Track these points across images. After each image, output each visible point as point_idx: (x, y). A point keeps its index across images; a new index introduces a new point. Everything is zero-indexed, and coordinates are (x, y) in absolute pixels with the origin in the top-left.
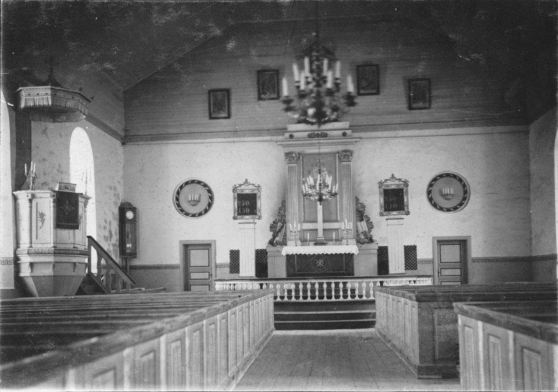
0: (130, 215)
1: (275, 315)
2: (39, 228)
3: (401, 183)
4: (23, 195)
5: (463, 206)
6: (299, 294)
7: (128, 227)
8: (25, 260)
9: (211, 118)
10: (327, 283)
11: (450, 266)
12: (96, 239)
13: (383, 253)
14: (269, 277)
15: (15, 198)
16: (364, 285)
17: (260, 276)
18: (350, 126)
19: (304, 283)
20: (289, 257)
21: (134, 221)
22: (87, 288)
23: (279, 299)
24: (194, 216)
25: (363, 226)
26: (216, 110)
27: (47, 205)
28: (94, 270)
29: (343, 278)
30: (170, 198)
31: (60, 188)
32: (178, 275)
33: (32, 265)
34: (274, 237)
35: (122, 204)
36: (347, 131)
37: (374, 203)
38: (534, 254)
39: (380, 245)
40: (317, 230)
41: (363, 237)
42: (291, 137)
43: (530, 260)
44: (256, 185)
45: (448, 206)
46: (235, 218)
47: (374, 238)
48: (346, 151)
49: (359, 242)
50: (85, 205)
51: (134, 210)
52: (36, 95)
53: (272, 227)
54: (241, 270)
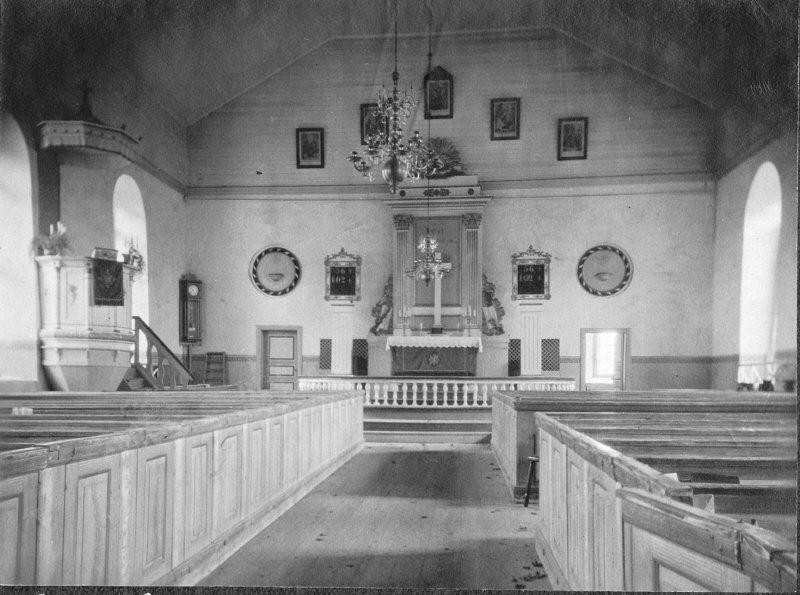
0: (193, 290)
1: (365, 423)
6: (412, 397)
7: (190, 307)
8: (51, 345)
9: (299, 166)
12: (147, 323)
13: (515, 345)
14: (369, 375)
15: (38, 266)
16: (485, 388)
17: (360, 374)
18: (479, 182)
20: (394, 349)
21: (198, 299)
22: (135, 383)
23: (368, 404)
25: (491, 312)
26: (305, 155)
27: (82, 280)
28: (143, 361)
30: (246, 267)
31: (97, 254)
32: (255, 367)
33: (60, 351)
35: (184, 276)
37: (507, 281)
38: (716, 353)
40: (433, 316)
41: (490, 326)
43: (709, 361)
47: (504, 329)
49: (486, 332)
51: (198, 283)
52: (59, 134)
53: (376, 311)
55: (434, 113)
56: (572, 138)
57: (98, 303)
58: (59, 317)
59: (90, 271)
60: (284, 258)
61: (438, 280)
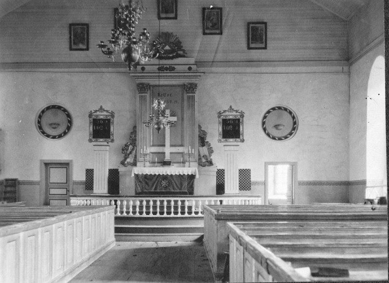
3: (238, 114)
5: (292, 136)
9: (71, 49)
10: (181, 201)
13: (221, 174)
14: (195, 195)
19: (182, 201)
20: (137, 176)
24: (54, 137)
25: (204, 150)
29: (154, 197)
39: (218, 168)
42: (143, 69)
43: (348, 184)
44: (110, 111)
45: (280, 135)
47: (213, 162)
48: (191, 84)
49: (201, 164)
54: (94, 188)
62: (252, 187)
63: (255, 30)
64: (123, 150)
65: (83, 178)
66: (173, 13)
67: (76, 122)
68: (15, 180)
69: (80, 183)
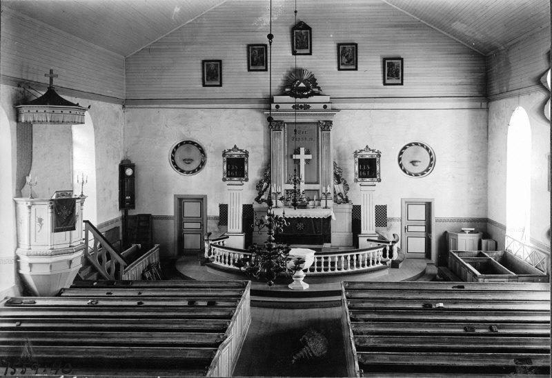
0: (129, 172)
2: (37, 231)
4: (23, 204)
8: (25, 262)
11: (416, 223)
13: (356, 211)
15: (16, 203)
21: (133, 176)
27: (46, 213)
31: (58, 196)
33: (31, 265)
34: (260, 195)
35: (122, 162)
36: (327, 104)
37: (352, 168)
41: (339, 198)
42: (277, 107)
46: (224, 180)
48: (326, 121)
50: (82, 204)
51: (133, 166)
55: (298, 52)
56: (393, 70)
57: (57, 231)
58: (30, 240)
59: (52, 208)
60: (194, 148)
61: (303, 164)
62: (388, 223)
63: (391, 65)
64: (257, 187)
65: (217, 213)
66: (548, 282)
67: (210, 159)
68: (149, 216)
69: (215, 218)
